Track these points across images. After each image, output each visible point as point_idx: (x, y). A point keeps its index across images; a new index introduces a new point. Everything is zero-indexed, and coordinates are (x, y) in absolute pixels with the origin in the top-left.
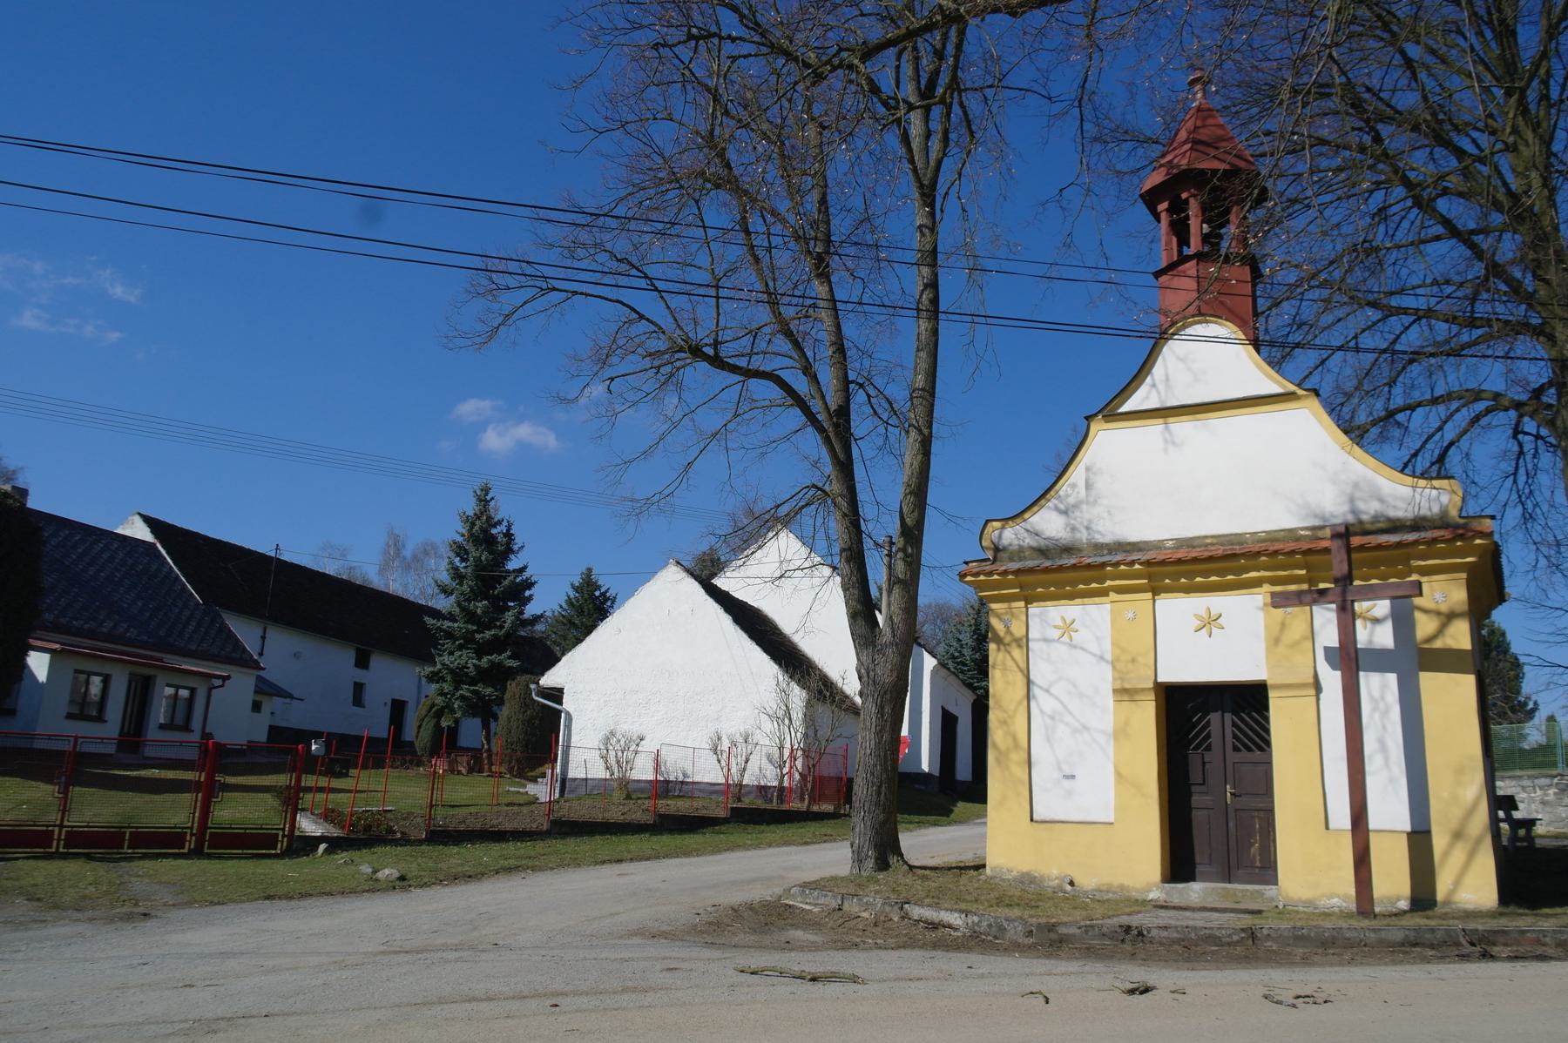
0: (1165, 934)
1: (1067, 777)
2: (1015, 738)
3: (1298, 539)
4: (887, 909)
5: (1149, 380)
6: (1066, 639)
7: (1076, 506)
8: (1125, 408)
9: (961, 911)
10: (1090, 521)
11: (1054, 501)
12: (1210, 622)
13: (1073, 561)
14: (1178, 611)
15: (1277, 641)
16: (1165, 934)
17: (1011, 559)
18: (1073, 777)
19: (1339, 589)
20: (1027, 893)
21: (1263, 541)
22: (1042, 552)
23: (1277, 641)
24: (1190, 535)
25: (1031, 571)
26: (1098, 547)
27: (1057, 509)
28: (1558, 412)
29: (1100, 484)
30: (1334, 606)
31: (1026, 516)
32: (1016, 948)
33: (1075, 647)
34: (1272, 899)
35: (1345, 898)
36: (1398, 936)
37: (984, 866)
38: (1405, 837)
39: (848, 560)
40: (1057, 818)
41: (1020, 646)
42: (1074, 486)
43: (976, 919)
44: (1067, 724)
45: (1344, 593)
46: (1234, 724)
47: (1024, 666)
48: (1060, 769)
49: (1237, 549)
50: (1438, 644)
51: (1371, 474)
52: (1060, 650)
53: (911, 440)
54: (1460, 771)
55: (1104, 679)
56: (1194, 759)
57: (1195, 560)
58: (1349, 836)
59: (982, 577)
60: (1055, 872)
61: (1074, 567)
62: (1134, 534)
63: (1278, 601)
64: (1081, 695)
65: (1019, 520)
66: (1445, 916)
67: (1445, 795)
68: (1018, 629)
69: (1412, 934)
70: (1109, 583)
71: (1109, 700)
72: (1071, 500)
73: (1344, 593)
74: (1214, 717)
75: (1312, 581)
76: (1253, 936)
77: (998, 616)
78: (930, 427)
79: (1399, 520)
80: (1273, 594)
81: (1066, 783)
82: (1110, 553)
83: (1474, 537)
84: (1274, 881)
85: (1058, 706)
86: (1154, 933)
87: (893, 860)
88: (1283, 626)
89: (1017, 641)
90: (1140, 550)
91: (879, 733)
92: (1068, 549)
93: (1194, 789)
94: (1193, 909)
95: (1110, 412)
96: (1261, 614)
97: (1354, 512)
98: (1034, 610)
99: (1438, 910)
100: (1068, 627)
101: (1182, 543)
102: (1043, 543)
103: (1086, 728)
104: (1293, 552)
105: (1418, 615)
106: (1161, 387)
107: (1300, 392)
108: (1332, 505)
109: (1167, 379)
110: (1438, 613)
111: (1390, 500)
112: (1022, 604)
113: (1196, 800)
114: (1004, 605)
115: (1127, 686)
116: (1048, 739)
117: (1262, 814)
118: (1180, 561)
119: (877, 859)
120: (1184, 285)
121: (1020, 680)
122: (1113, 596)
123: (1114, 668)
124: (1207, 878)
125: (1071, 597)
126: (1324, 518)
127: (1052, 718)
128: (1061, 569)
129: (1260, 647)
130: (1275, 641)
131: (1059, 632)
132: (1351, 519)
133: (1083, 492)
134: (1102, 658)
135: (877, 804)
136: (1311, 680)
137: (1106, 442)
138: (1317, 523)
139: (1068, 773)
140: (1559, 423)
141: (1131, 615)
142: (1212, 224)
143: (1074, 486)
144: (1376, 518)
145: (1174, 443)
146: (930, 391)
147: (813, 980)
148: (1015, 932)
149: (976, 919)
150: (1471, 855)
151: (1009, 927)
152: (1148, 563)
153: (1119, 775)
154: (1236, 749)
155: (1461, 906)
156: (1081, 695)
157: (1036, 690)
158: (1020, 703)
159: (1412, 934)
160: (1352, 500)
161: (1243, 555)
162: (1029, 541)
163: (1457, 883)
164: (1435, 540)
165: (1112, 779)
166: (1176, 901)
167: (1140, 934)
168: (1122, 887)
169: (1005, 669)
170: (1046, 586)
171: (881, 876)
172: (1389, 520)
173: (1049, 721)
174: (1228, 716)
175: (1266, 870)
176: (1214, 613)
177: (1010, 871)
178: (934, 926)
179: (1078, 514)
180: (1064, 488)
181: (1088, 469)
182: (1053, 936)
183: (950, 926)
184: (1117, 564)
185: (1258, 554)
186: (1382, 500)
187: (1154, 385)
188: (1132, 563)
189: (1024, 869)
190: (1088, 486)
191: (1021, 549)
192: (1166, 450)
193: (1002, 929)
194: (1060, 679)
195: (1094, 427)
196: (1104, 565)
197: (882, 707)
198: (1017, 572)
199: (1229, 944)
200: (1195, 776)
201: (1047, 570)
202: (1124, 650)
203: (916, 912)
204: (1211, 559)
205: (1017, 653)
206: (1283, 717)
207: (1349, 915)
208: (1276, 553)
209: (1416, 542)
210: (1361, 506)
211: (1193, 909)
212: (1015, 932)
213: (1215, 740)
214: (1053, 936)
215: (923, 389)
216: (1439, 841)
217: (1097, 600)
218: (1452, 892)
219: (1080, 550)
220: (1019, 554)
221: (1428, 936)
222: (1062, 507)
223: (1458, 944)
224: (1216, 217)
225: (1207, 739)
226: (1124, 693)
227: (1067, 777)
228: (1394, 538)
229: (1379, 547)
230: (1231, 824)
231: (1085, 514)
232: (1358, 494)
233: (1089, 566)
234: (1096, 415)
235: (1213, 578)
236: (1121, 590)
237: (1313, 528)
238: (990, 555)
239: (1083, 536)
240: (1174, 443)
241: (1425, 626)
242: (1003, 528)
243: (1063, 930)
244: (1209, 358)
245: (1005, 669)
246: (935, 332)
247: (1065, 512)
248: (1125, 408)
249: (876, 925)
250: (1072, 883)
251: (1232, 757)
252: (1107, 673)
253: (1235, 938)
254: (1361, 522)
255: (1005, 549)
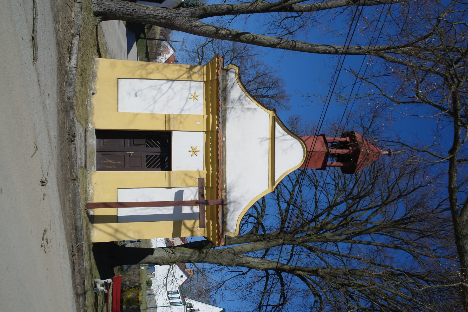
0: (73, 150)
1: (136, 93)
2: (151, 73)
3: (222, 184)
4: (76, 27)
5: (286, 133)
6: (190, 96)
7: (242, 104)
8: (276, 124)
9: (77, 65)
10: (235, 109)
11: (244, 95)
12: (194, 151)
13: (220, 103)
14: (199, 140)
15: (186, 175)
16: (73, 150)
17: (223, 76)
18: (136, 96)
19: (203, 201)
20: (87, 76)
21: (223, 172)
22: (225, 89)
23: (186, 175)
24: (227, 146)
25: (218, 86)
26: (225, 111)
27: (241, 96)
28: (256, 235)
29: (249, 114)
30: (198, 200)
31: (239, 83)
32: (61, 93)
33: (187, 100)
34: (91, 169)
35: (92, 199)
36: (79, 224)
37: (100, 56)
38: (116, 214)
39: (228, 8)
40: (119, 89)
41: (188, 77)
42: (249, 103)
43: (74, 72)
44: (157, 95)
45: (202, 203)
46: (156, 156)
47: (180, 79)
48: (139, 91)
49: (220, 164)
50: (183, 227)
51: (243, 208)
52: (186, 94)
53: (275, 39)
54: (139, 232)
55: (173, 111)
56: (143, 141)
57: (217, 149)
58: (116, 201)
59: (217, 65)
60: (97, 87)
61: (218, 103)
62: (228, 125)
63: (201, 181)
64: (168, 101)
65: (238, 80)
66: (87, 228)
67: (130, 227)
68: (195, 77)
69: (80, 229)
70: (211, 115)
71: (166, 112)
72: (244, 102)
73: (202, 203)
74: (159, 149)
75: (207, 188)
76: (75, 180)
77: (201, 69)
78: (280, 48)
79: (226, 217)
80: (203, 179)
81: (133, 93)
82: (222, 116)
83: (219, 241)
84: (98, 169)
85: (164, 91)
86: (73, 146)
87: (99, 18)
88: (192, 177)
89: (190, 77)
90: (223, 127)
91: (154, 17)
92: (225, 99)
93: (132, 140)
94: (85, 143)
95: (275, 119)
96: (196, 170)
97: (230, 202)
98: (202, 84)
99: (90, 225)
100: (195, 97)
101: (224, 143)
102: (228, 89)
103: (155, 102)
104: (218, 184)
105: (193, 221)
106: (283, 138)
107: (274, 187)
108: (233, 195)
109: (285, 140)
110: (193, 228)
111: (233, 214)
112: (205, 80)
113: (128, 141)
114: (205, 72)
115: (171, 120)
116: (151, 87)
117: (123, 164)
118: (217, 144)
119: (99, 12)
120: (320, 147)
121: (175, 77)
122: (206, 116)
123: (178, 115)
124: (98, 144)
125: (207, 99)
126: (229, 193)
127: (159, 89)
128: (218, 98)
129: (184, 169)
130: (186, 174)
131: (193, 94)
132: (228, 201)
133: (246, 107)
134: (182, 110)
135: (123, 13)
136: (171, 186)
137: (264, 116)
138: (227, 190)
139: (137, 94)
140: (252, 235)
141: (198, 123)
142: (338, 151)
143: (249, 103)
144: (227, 209)
145: (261, 141)
146: (293, 48)
147: (33, 38)
148: (69, 91)
149: (74, 72)
150: (110, 235)
151: (71, 89)
152: (218, 132)
153: (137, 114)
154: (147, 156)
155: (92, 232)
156: (168, 101)
157: (170, 83)
158: (166, 76)
159: (80, 229)
160: (234, 202)
161: (218, 167)
162: (230, 84)
163: (100, 230)
164: (218, 230)
165: (135, 112)
166: (88, 134)
167: (72, 141)
168: (93, 114)
169: (179, 70)
170: (212, 90)
171: (92, 15)
172: (227, 213)
173: (158, 87)
174: (159, 154)
175: (102, 167)
176: (197, 153)
177: (97, 68)
178: (70, 52)
179: (238, 104)
180: (249, 99)
181: (255, 109)
182: (69, 108)
183: (70, 59)
184: (218, 120)
185: (218, 172)
186: (233, 211)
187: (284, 135)
188: (218, 126)
189: (99, 74)
190: (249, 109)
191: (227, 80)
192: (259, 138)
193: (71, 85)
194: (175, 93)
195: (271, 112)
196: (218, 115)
197: (165, 19)
198: (218, 80)
199: (71, 172)
200: (137, 141)
201: (218, 92)
202: (185, 119)
203: (76, 42)
204: (218, 155)
205: (186, 76)
206: (158, 176)
207: (86, 199)
208: (218, 178)
209: (218, 224)
210: (232, 205)
211: (85, 143)
212: (69, 91)
213: (150, 149)
214: (69, 108)
215: (295, 46)
216: (115, 225)
217: (205, 109)
218: (97, 228)
219: (224, 104)
220: (225, 79)
221: (79, 233)
222: (242, 98)
223: (77, 242)
224: (340, 158)
225: (149, 148)
226: (168, 119)
227: (136, 93)
228: (220, 216)
229: (218, 212)
230: (119, 153)
231: (238, 107)
232: (236, 204)
233: (218, 109)
234: (276, 114)
235: (210, 154)
236: (208, 119)
237: (226, 189)
238: (225, 67)
239: (230, 105)
240: (261, 141)
241: (189, 223)
242: (236, 73)
243: (71, 112)
244: (292, 155)
245: (179, 70)
246: (318, 52)
247: (239, 99)
248: (277, 124)
249: (68, 22)
250: (93, 94)
251: (144, 154)
252: (176, 112)
253: (74, 174)
254: (226, 205)
255: (227, 74)
